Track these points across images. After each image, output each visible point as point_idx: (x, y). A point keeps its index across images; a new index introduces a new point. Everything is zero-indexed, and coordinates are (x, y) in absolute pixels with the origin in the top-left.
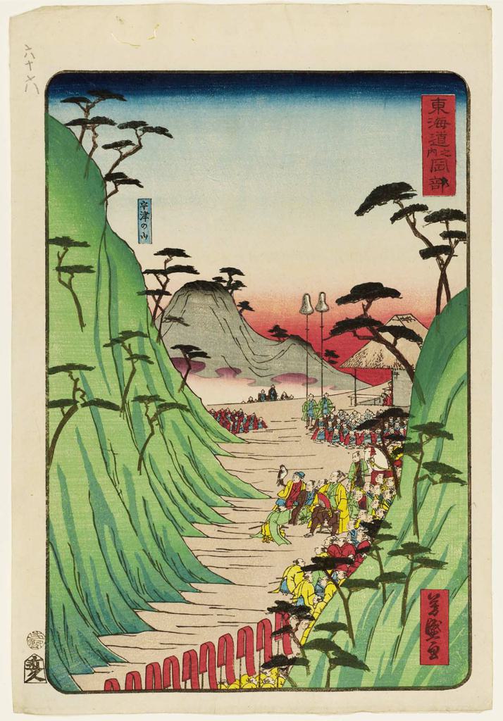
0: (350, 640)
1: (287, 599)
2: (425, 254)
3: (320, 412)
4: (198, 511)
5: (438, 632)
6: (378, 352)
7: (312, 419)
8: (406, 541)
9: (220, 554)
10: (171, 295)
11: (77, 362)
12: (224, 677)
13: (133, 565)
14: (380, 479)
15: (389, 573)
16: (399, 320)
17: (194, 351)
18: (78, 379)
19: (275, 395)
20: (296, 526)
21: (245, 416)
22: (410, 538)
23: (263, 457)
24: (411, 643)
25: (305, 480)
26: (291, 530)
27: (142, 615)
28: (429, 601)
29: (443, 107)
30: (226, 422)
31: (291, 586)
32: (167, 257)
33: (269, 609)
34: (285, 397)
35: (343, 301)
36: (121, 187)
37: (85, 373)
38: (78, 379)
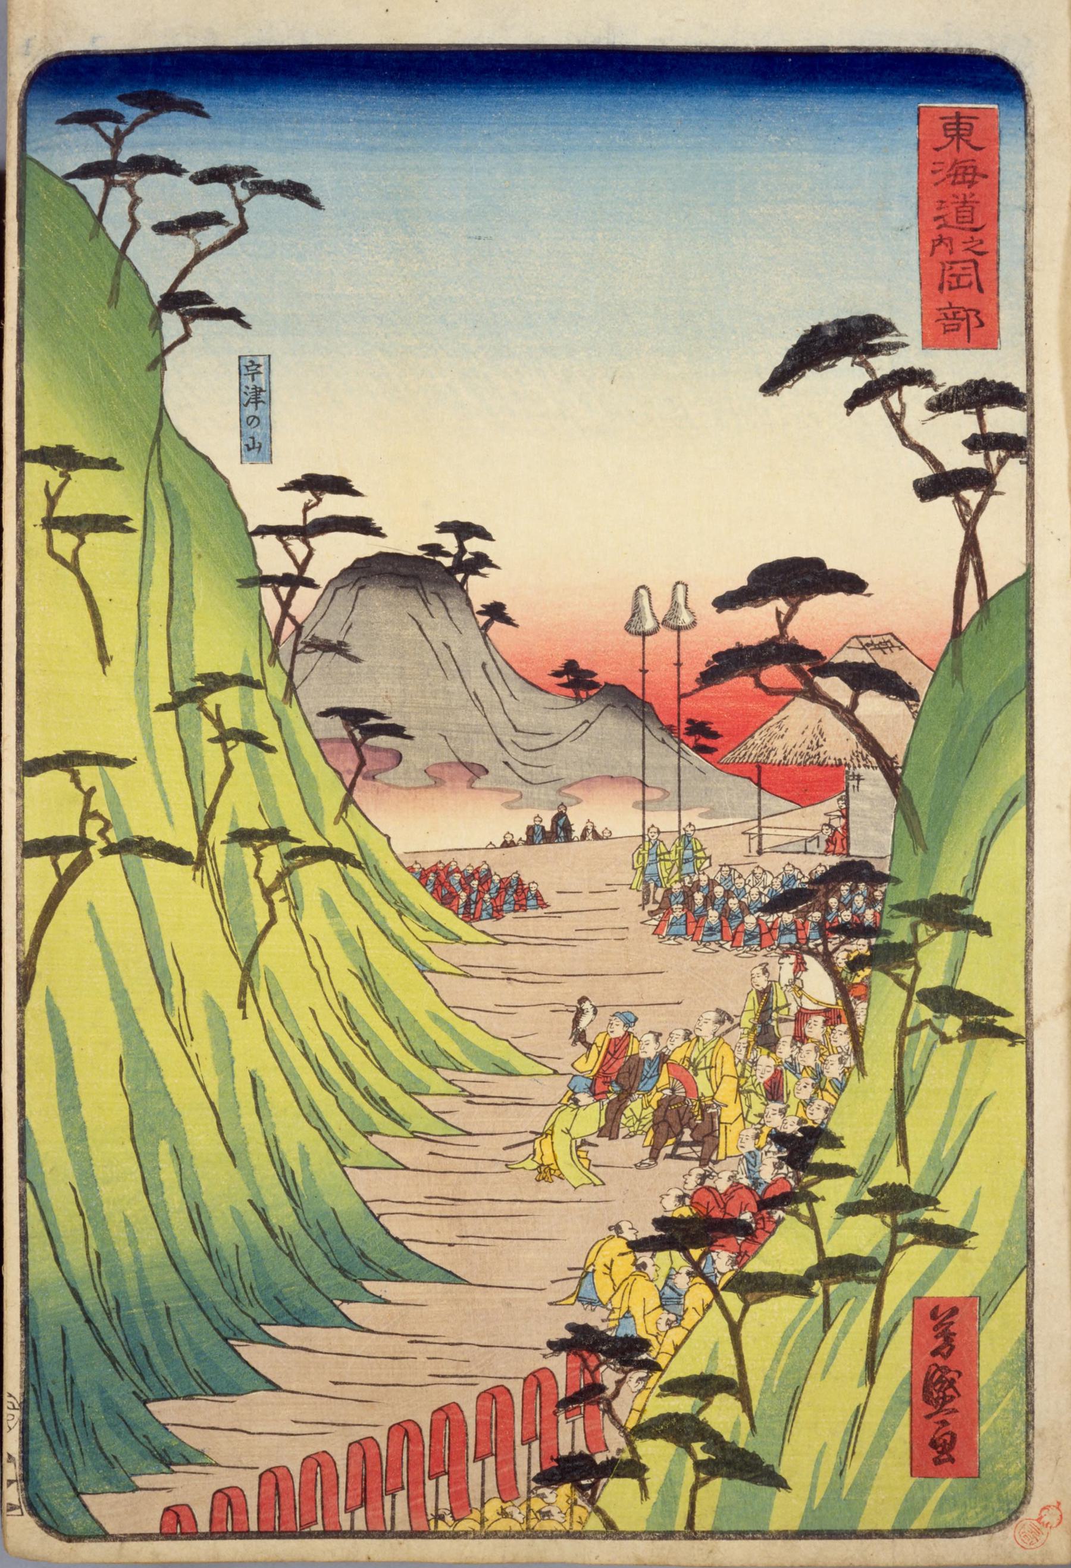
0: (744, 1419)
1: (595, 1319)
2: (927, 490)
3: (675, 869)
4: (381, 1104)
5: (952, 1398)
6: (814, 723)
7: (656, 886)
8: (877, 1181)
9: (436, 1210)
10: (315, 586)
11: (93, 748)
12: (444, 1503)
13: (224, 1233)
14: (815, 1028)
15: (840, 1259)
16: (864, 648)
17: (373, 721)
18: (93, 790)
19: (567, 829)
20: (614, 1142)
21: (496, 878)
22: (889, 1173)
23: (537, 978)
24: (891, 1412)
25: (636, 1029)
26: (606, 1150)
27: (248, 1352)
28: (933, 1323)
29: (969, 135)
30: (450, 893)
31: (603, 1288)
32: (307, 496)
33: (550, 1344)
34: (592, 834)
35: (727, 602)
36: (199, 326)
37: (112, 771)
38: (93, 790)
